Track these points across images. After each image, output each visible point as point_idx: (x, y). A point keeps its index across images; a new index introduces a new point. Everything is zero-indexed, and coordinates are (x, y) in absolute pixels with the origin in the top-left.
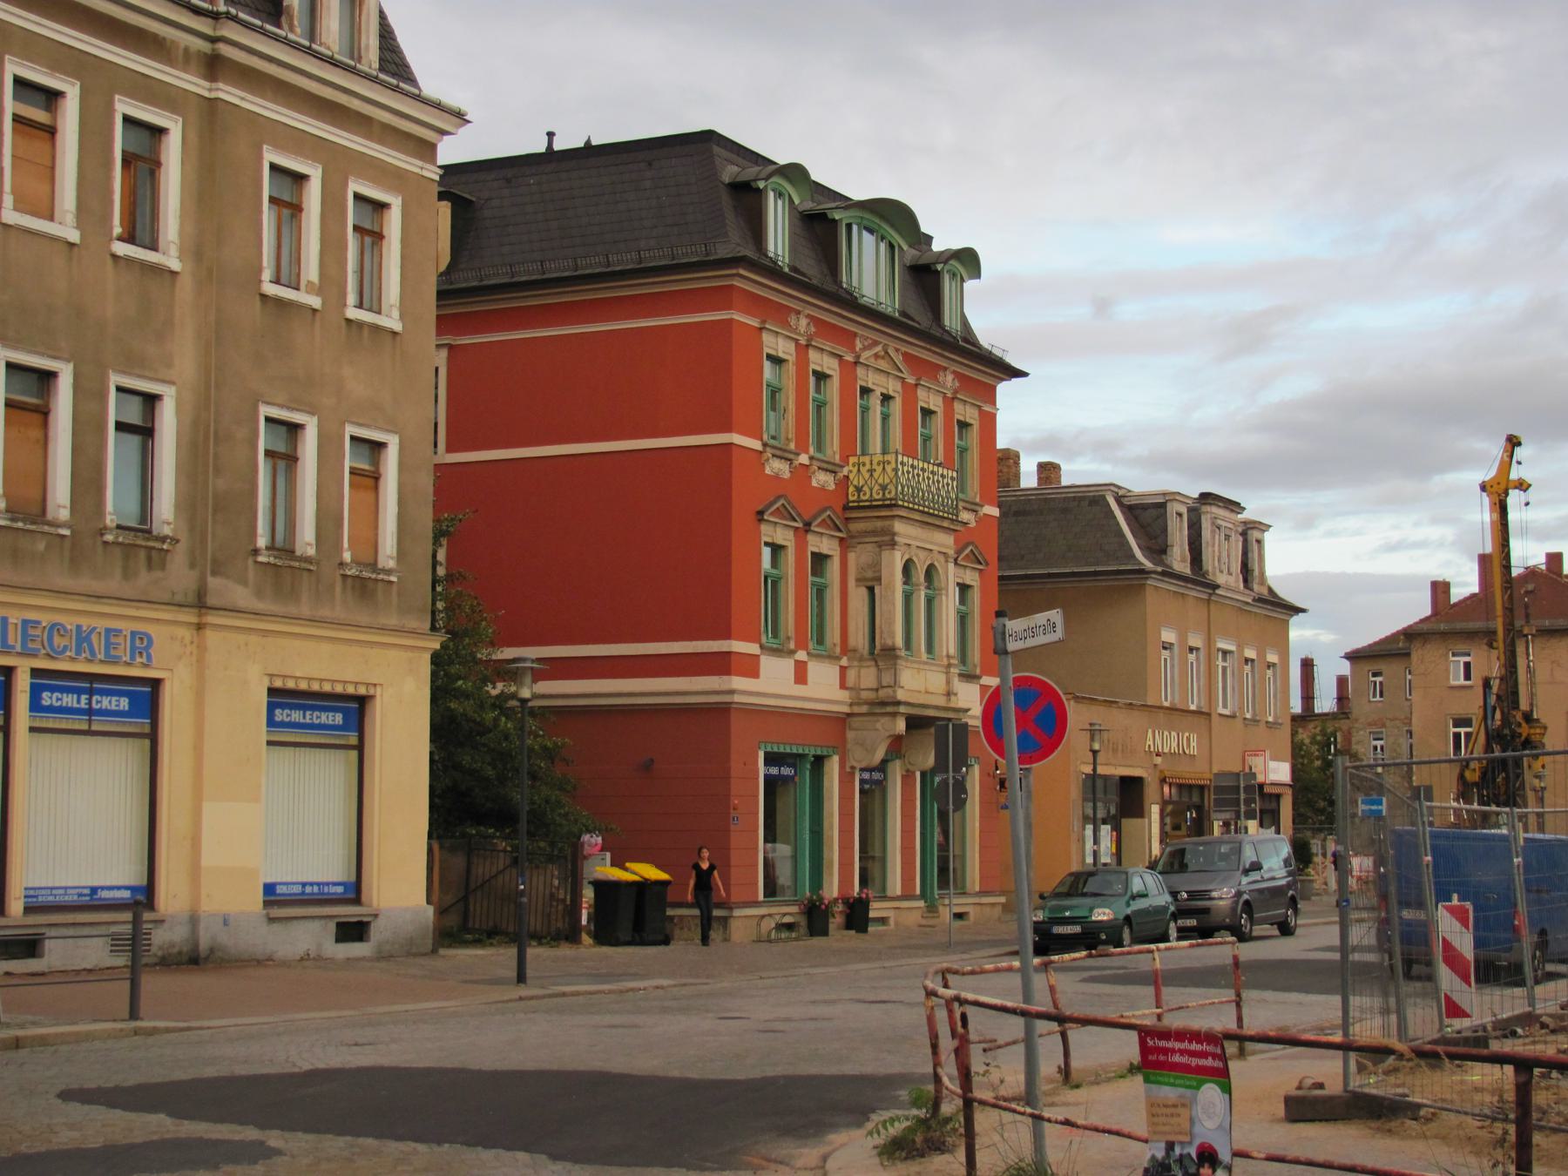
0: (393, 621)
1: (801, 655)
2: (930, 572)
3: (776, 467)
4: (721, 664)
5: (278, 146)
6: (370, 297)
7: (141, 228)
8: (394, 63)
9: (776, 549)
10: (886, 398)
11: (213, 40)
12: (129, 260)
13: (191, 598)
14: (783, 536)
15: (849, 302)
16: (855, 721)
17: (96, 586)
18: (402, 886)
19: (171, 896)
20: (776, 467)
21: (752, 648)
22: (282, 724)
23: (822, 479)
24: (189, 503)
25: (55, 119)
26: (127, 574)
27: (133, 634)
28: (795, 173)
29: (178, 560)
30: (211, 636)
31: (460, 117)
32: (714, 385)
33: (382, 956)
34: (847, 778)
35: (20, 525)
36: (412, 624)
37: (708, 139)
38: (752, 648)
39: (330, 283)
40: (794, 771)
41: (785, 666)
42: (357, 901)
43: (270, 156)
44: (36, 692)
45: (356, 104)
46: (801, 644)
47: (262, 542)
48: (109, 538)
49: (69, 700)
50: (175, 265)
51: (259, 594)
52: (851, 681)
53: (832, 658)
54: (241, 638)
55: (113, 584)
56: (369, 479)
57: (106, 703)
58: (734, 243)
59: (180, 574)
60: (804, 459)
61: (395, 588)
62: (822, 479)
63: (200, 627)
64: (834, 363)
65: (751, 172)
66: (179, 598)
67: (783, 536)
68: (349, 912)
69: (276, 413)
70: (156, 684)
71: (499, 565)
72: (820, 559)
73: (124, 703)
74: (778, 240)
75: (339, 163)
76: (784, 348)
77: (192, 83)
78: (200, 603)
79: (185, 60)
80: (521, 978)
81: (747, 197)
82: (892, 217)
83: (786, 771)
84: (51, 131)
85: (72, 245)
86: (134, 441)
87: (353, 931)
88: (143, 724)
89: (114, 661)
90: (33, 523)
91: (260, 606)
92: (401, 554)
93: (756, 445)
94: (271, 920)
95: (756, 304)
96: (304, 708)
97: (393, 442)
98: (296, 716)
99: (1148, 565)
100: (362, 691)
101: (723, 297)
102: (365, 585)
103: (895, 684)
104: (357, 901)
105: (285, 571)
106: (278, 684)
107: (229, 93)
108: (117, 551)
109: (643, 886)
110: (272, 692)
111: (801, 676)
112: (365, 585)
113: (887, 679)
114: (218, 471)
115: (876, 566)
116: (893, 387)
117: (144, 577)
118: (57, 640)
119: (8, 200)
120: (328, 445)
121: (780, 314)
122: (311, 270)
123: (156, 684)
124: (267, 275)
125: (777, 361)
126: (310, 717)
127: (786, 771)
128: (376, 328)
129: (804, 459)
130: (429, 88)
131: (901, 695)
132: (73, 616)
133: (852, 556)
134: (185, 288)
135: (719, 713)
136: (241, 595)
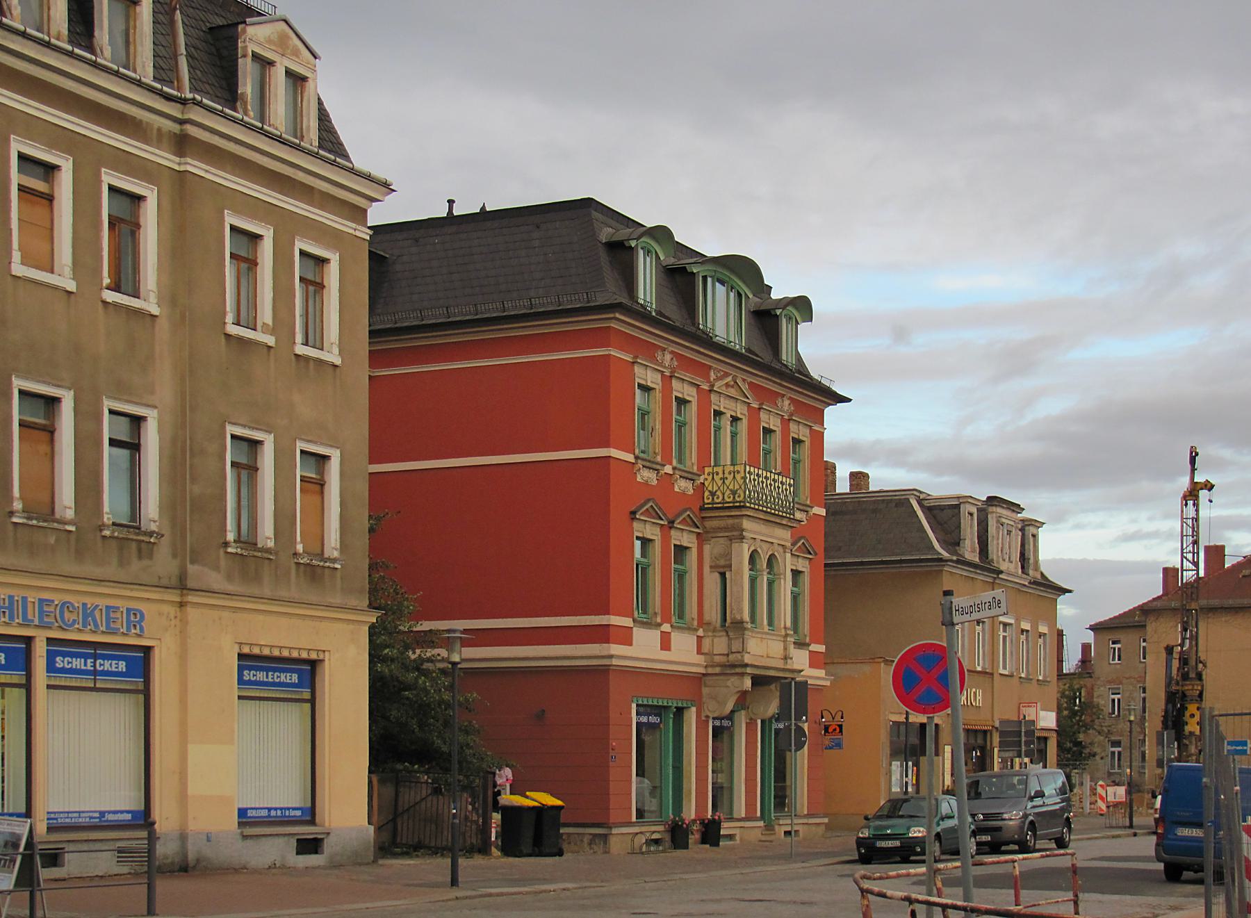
0: (337, 600)
1: (666, 627)
2: (771, 559)
3: (646, 476)
4: (602, 634)
5: (237, 211)
6: (314, 336)
7: (125, 279)
8: (330, 141)
9: (645, 542)
10: (735, 419)
11: (182, 122)
12: (116, 305)
13: (174, 581)
14: (652, 532)
15: (706, 341)
16: (708, 679)
17: (98, 572)
18: (348, 809)
19: (165, 817)
20: (646, 476)
21: (627, 622)
22: (250, 682)
23: (682, 485)
24: (171, 505)
25: (52, 188)
26: (123, 563)
27: (128, 610)
28: (662, 234)
29: (163, 549)
30: (191, 612)
31: (386, 186)
32: (593, 406)
33: (335, 865)
34: (702, 725)
35: (34, 522)
36: (353, 602)
37: (588, 203)
38: (627, 622)
39: (282, 325)
40: (664, 717)
41: (654, 636)
42: (312, 822)
43: (230, 219)
44: (51, 657)
45: (301, 176)
46: (666, 619)
47: (231, 537)
48: (107, 533)
49: (77, 663)
50: (155, 310)
51: (229, 577)
52: (705, 649)
53: (690, 629)
54: (215, 614)
55: (111, 571)
56: (316, 485)
57: (107, 665)
58: (611, 292)
59: (164, 563)
60: (668, 469)
61: (338, 574)
62: (682, 485)
63: (182, 605)
64: (693, 391)
65: (623, 234)
66: (165, 582)
67: (652, 532)
68: (307, 831)
69: (239, 431)
70: (147, 650)
71: (416, 556)
72: (681, 550)
73: (122, 666)
74: (647, 288)
75: (287, 225)
76: (652, 378)
77: (166, 158)
78: (182, 585)
79: (158, 138)
80: (454, 882)
81: (621, 253)
82: (741, 270)
83: (653, 719)
84: (50, 198)
85: (70, 293)
86: (124, 453)
87: (310, 846)
88: (17, 677)
89: (114, 633)
90: (45, 521)
91: (230, 588)
92: (344, 546)
93: (630, 458)
94: (245, 837)
95: (630, 343)
96: (267, 670)
97: (335, 455)
98: (261, 676)
99: (945, 554)
100: (314, 656)
101: (602, 337)
102: (314, 571)
103: (743, 651)
104: (312, 822)
105: (250, 560)
106: (246, 650)
107: (195, 167)
108: (114, 543)
109: (541, 811)
110: (241, 656)
111: (666, 644)
112: (314, 571)
113: (736, 646)
114: (194, 480)
115: (728, 555)
116: (741, 410)
117: (136, 566)
118: (67, 614)
119: (16, 256)
120: (87, 415)
121: (649, 351)
122: (266, 314)
123: (147, 650)
124: (230, 318)
125: (645, 389)
126: (272, 677)
127: (653, 719)
128: (320, 362)
129: (668, 469)
130: (359, 162)
131: (747, 659)
132: (79, 595)
133: (707, 548)
134: (163, 327)
135: (600, 674)
136: (215, 580)
